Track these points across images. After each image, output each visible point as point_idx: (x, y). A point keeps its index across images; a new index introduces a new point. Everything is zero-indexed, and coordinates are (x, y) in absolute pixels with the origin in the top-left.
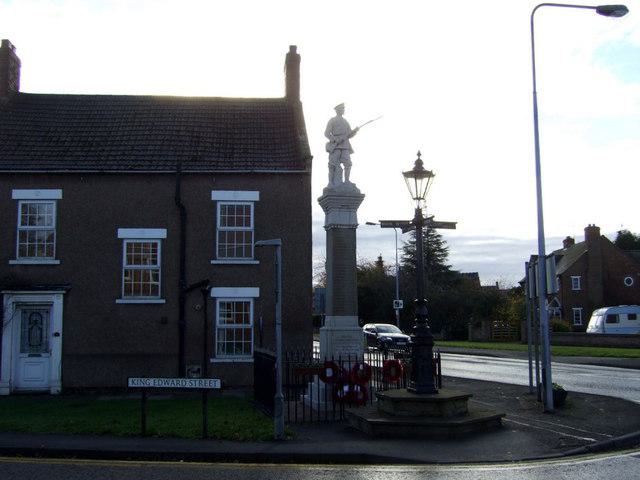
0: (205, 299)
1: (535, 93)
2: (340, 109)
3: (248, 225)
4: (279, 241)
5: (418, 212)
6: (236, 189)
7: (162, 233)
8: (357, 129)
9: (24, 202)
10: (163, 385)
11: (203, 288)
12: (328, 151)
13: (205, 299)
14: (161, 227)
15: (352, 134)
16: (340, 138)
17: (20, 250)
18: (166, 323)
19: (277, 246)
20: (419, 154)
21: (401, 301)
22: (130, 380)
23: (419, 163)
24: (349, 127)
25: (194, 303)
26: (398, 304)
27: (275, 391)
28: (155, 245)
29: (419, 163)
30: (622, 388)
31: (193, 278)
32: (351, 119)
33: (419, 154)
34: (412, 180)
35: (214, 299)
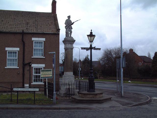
0: (30, 67)
1: (121, 15)
2: (69, 17)
3: (42, 47)
4: (55, 53)
5: (91, 45)
6: (39, 37)
7: (18, 49)
8: (74, 23)
9: (35, 41)
10: (23, 90)
11: (29, 65)
12: (65, 28)
13: (30, 67)
14: (18, 48)
15: (73, 24)
16: (69, 24)
17: (16, 56)
18: (60, 76)
19: (54, 54)
20: (91, 30)
21: (80, 68)
22: (14, 89)
23: (91, 33)
24: (71, 22)
25: (27, 68)
26: (80, 69)
27: (53, 91)
28: (16, 52)
29: (91, 33)
30: (151, 92)
31: (26, 62)
32: (72, 20)
33: (91, 30)
34: (89, 37)
35: (33, 67)
